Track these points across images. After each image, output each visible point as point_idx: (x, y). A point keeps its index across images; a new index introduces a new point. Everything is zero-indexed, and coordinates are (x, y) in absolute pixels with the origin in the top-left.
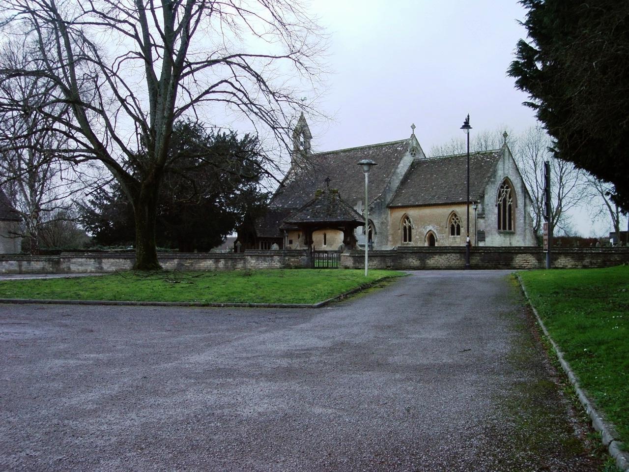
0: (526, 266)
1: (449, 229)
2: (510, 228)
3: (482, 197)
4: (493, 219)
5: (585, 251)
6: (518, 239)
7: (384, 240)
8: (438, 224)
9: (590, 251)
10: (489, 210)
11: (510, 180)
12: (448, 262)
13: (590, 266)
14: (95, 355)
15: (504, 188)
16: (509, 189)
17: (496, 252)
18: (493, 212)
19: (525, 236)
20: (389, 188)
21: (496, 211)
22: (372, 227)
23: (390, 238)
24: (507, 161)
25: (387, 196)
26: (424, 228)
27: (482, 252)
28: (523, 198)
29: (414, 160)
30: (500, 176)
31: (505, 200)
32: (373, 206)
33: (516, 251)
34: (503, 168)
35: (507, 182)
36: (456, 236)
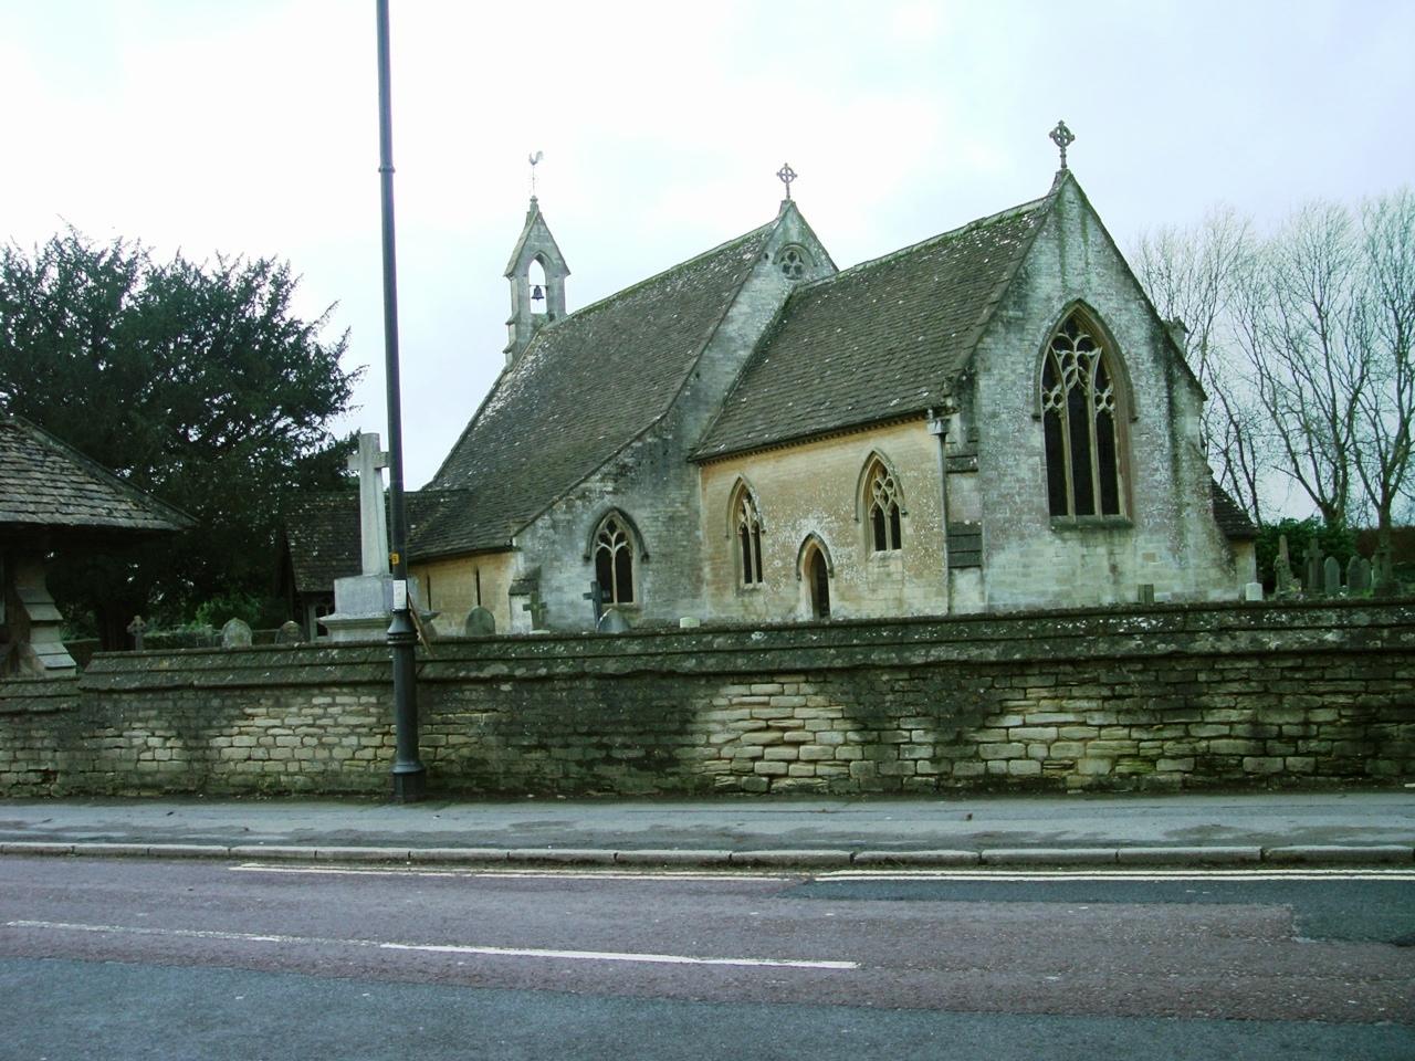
0: (780, 768)
1: (866, 524)
2: (1110, 505)
3: (965, 385)
4: (1025, 473)
5: (1204, 644)
6: (1151, 548)
7: (684, 581)
8: (832, 510)
9: (1243, 642)
10: (1004, 438)
11: (1094, 311)
12: (322, 745)
13: (1249, 763)
14: (66, 925)
15: (1070, 347)
16: (1097, 352)
17: (582, 676)
18: (1021, 446)
19: (1180, 534)
20: (696, 392)
21: (1037, 438)
22: (630, 534)
23: (707, 572)
24: (1074, 240)
25: (689, 419)
26: (793, 528)
27: (497, 679)
28: (1163, 383)
29: (795, 288)
30: (1049, 299)
31: (1078, 395)
32: (630, 461)
33: (711, 663)
34: (1057, 268)
35: (1078, 324)
36: (889, 551)
